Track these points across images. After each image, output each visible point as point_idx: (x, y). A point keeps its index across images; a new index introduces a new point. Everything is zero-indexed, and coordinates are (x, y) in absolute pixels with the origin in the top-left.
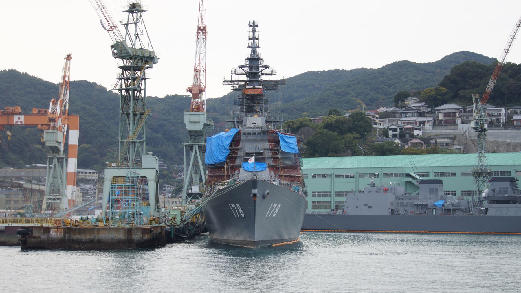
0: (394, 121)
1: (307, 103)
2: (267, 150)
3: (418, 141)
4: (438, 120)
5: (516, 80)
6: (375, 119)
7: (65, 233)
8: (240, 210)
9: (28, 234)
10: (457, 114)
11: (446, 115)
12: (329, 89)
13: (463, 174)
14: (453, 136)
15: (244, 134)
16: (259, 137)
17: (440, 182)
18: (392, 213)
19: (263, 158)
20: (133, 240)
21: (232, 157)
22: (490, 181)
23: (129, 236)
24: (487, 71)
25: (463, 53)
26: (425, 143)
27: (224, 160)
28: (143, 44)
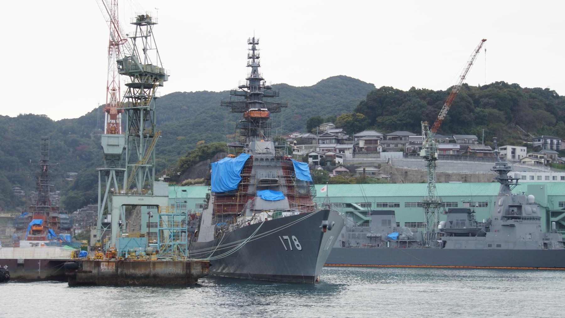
0: (311, 147)
1: (181, 127)
2: (282, 177)
3: (343, 169)
4: (358, 147)
5: (436, 108)
6: (293, 145)
7: (117, 267)
8: (297, 243)
9: (77, 268)
10: (379, 141)
11: (367, 142)
12: (204, 112)
13: (407, 205)
14: (377, 165)
15: (257, 159)
16: (273, 164)
17: (392, 213)
18: (344, 246)
19: (277, 186)
20: (192, 275)
21: (244, 184)
22: (446, 213)
23: (188, 271)
24: (405, 97)
25: (340, 77)
26: (350, 171)
27: (236, 187)
28: (151, 60)
